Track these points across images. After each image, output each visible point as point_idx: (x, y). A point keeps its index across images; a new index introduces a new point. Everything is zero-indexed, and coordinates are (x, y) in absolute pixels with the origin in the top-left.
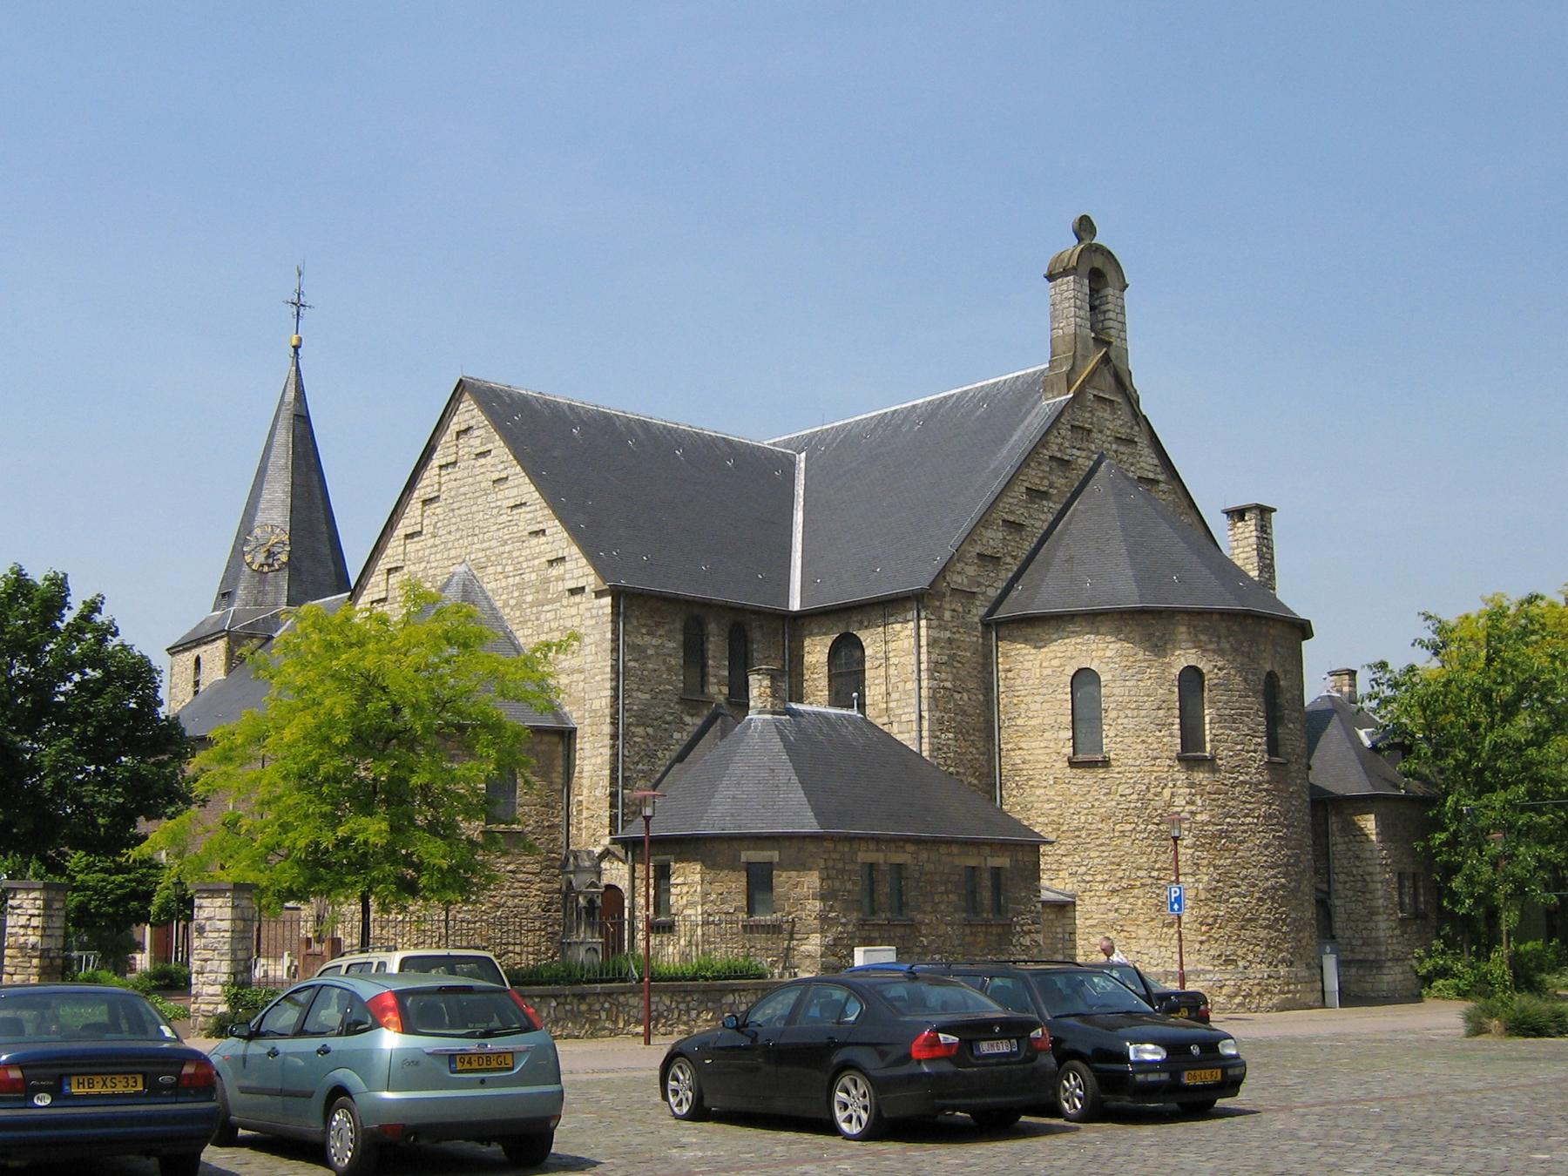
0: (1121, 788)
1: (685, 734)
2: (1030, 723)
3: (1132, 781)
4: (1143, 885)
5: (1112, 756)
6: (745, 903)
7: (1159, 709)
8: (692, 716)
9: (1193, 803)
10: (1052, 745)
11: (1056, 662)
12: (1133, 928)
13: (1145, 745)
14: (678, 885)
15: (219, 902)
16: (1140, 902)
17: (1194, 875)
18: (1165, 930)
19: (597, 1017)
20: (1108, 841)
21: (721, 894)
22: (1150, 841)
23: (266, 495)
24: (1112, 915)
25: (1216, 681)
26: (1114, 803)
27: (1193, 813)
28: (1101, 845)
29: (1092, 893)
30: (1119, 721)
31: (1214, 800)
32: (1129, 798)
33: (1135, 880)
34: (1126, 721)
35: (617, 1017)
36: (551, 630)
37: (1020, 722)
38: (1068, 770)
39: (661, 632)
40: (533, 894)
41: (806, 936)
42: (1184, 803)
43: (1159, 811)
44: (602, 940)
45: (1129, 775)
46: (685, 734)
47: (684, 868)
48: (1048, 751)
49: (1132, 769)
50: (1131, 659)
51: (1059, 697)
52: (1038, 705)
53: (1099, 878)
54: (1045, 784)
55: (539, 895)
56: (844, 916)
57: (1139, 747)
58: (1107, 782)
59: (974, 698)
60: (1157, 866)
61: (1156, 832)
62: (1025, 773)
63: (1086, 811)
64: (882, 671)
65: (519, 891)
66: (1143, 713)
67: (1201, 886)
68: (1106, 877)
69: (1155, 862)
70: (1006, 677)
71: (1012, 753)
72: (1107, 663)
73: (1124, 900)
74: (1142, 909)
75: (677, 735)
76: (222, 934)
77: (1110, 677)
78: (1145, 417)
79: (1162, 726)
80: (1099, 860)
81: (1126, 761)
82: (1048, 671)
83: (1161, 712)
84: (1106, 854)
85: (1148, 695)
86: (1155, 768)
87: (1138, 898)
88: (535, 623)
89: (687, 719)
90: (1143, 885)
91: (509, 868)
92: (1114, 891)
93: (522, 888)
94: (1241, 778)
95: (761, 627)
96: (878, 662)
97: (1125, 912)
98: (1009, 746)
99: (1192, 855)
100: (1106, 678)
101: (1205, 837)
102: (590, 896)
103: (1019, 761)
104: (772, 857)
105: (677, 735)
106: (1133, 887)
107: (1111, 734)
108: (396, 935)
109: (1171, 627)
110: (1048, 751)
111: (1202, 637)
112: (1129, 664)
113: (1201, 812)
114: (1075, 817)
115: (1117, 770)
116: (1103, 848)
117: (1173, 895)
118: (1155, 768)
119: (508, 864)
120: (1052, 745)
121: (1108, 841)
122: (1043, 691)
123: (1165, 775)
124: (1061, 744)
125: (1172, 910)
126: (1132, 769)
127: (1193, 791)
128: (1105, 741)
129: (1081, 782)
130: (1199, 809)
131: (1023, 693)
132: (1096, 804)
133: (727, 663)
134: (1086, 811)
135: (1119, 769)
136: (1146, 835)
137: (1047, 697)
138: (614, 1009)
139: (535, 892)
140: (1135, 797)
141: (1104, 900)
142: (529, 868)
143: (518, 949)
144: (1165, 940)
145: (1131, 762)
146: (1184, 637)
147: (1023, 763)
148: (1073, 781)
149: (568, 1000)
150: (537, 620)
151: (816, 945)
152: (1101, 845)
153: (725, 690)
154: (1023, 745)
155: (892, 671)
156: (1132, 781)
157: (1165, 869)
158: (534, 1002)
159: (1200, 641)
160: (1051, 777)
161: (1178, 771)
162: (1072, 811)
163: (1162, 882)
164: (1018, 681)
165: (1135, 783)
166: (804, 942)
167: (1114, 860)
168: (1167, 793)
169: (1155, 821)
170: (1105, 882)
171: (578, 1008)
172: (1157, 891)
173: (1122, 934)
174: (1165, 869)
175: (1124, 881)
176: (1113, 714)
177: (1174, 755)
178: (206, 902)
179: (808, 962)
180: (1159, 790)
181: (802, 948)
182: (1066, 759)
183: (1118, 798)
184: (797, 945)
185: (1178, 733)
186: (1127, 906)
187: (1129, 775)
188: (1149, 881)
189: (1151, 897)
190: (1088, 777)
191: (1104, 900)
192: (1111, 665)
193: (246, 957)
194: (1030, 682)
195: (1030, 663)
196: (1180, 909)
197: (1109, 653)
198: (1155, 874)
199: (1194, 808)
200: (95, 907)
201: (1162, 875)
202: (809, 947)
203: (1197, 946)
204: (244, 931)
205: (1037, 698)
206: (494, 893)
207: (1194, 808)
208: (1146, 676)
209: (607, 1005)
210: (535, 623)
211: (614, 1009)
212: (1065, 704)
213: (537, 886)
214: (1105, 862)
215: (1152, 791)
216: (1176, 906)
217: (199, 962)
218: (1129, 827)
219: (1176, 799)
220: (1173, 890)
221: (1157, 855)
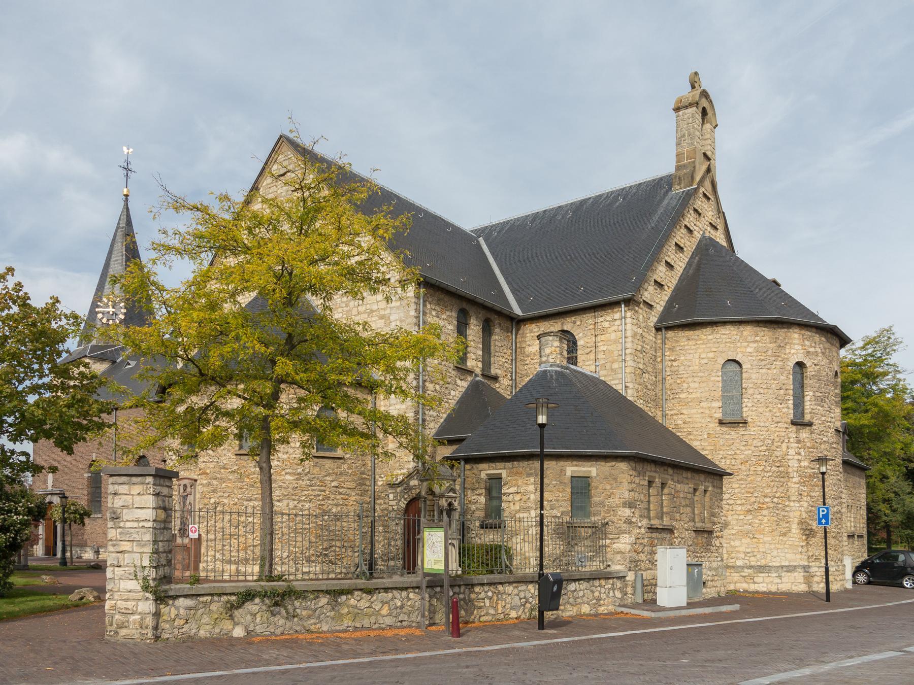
0: (755, 442)
1: (457, 392)
2: (690, 396)
3: (762, 437)
4: (768, 508)
5: (749, 420)
6: (570, 509)
7: (780, 389)
8: (461, 380)
9: (799, 454)
10: (707, 411)
11: (711, 355)
12: (762, 536)
13: (772, 413)
14: (510, 494)
15: (136, 489)
16: (766, 520)
17: (799, 502)
18: (781, 538)
19: (482, 604)
20: (745, 477)
21: (551, 501)
22: (773, 478)
23: (113, 259)
24: (747, 527)
25: (813, 373)
26: (750, 452)
27: (799, 461)
28: (741, 480)
29: (733, 513)
30: (755, 396)
31: (811, 452)
32: (761, 449)
33: (763, 504)
34: (759, 396)
35: (497, 604)
36: (359, 313)
37: (682, 396)
38: (718, 429)
39: (444, 316)
40: (350, 504)
41: (617, 536)
42: (794, 453)
43: (780, 458)
44: (459, 537)
45: (761, 433)
46: (457, 392)
47: (517, 480)
48: (704, 415)
49: (763, 429)
50: (763, 354)
51: (712, 379)
52: (697, 385)
53: (739, 502)
54: (700, 438)
55: (355, 505)
56: (640, 521)
57: (768, 414)
58: (746, 437)
59: (651, 378)
60: (777, 495)
61: (777, 472)
62: (685, 430)
63: (731, 457)
64: (592, 356)
65: (341, 502)
66: (770, 391)
67: (803, 509)
68: (743, 501)
69: (776, 492)
70: (672, 365)
71: (675, 417)
72: (747, 357)
73: (755, 517)
74: (767, 523)
75: (453, 393)
76: (141, 524)
77: (749, 366)
78: (723, 213)
79: (783, 401)
80: (739, 489)
81: (759, 423)
82: (705, 361)
83: (782, 392)
84: (744, 486)
85: (774, 379)
86: (778, 429)
87: (765, 516)
88: (345, 309)
89: (459, 382)
90: (768, 508)
91: (333, 484)
92: (749, 511)
93: (342, 499)
94: (824, 439)
95: (500, 324)
96: (589, 350)
97: (756, 525)
98: (673, 412)
99: (798, 488)
100: (747, 367)
101: (805, 477)
102: (450, 500)
103: (681, 422)
104: (590, 471)
105: (453, 393)
106: (761, 508)
107: (750, 405)
108: (246, 532)
109: (789, 334)
110: (704, 415)
111: (807, 343)
112: (762, 358)
113: (804, 460)
114: (723, 460)
115: (753, 429)
116: (742, 482)
117: (821, 513)
118: (778, 429)
119: (332, 481)
120: (707, 411)
121: (745, 477)
122: (700, 374)
123: (783, 434)
124: (714, 411)
125: (820, 523)
126: (763, 429)
127: (800, 446)
128: (745, 409)
129: (727, 437)
130: (803, 458)
131: (685, 376)
132: (738, 452)
133: (481, 346)
134: (731, 457)
135: (754, 429)
136: (771, 474)
137: (704, 379)
138: (495, 598)
139: (352, 503)
140: (764, 448)
141: (742, 517)
142: (348, 484)
143: (338, 544)
144: (781, 544)
145: (762, 424)
146: (796, 341)
147: (684, 423)
148: (722, 436)
149: (462, 590)
150: (347, 306)
151: (625, 543)
152: (741, 480)
153: (480, 365)
154: (684, 411)
155: (600, 356)
156: (762, 437)
157: (782, 497)
158: (436, 592)
159: (805, 345)
160: (706, 433)
161: (791, 432)
162: (721, 456)
163: (780, 506)
164: (682, 368)
165: (764, 438)
166: (616, 541)
167: (749, 490)
168: (784, 446)
169: (777, 464)
170: (743, 504)
171: (469, 596)
172: (777, 512)
173: (754, 540)
174: (782, 497)
175: (756, 504)
176: (750, 391)
177: (789, 421)
178: (123, 489)
179: (619, 557)
180: (780, 444)
181: (615, 546)
182: (717, 421)
183: (753, 448)
184: (611, 544)
185: (791, 406)
186: (757, 521)
187: (761, 433)
188: (772, 505)
189: (773, 516)
190: (732, 434)
191: (742, 517)
192: (751, 358)
193: (167, 549)
194: (691, 368)
195: (691, 356)
196: (827, 523)
197: (749, 350)
198: (775, 500)
199: (800, 457)
200: (14, 560)
201: (780, 501)
202: (620, 545)
203: (800, 549)
204: (165, 521)
205: (696, 379)
206: (323, 502)
207: (800, 457)
208: (773, 366)
209: (490, 594)
210: (345, 309)
211: (495, 598)
212: (717, 384)
213: (353, 498)
214: (743, 491)
215: (776, 444)
216: (823, 521)
217: (115, 555)
218: (760, 468)
219: (789, 450)
220: (821, 509)
221: (778, 487)
